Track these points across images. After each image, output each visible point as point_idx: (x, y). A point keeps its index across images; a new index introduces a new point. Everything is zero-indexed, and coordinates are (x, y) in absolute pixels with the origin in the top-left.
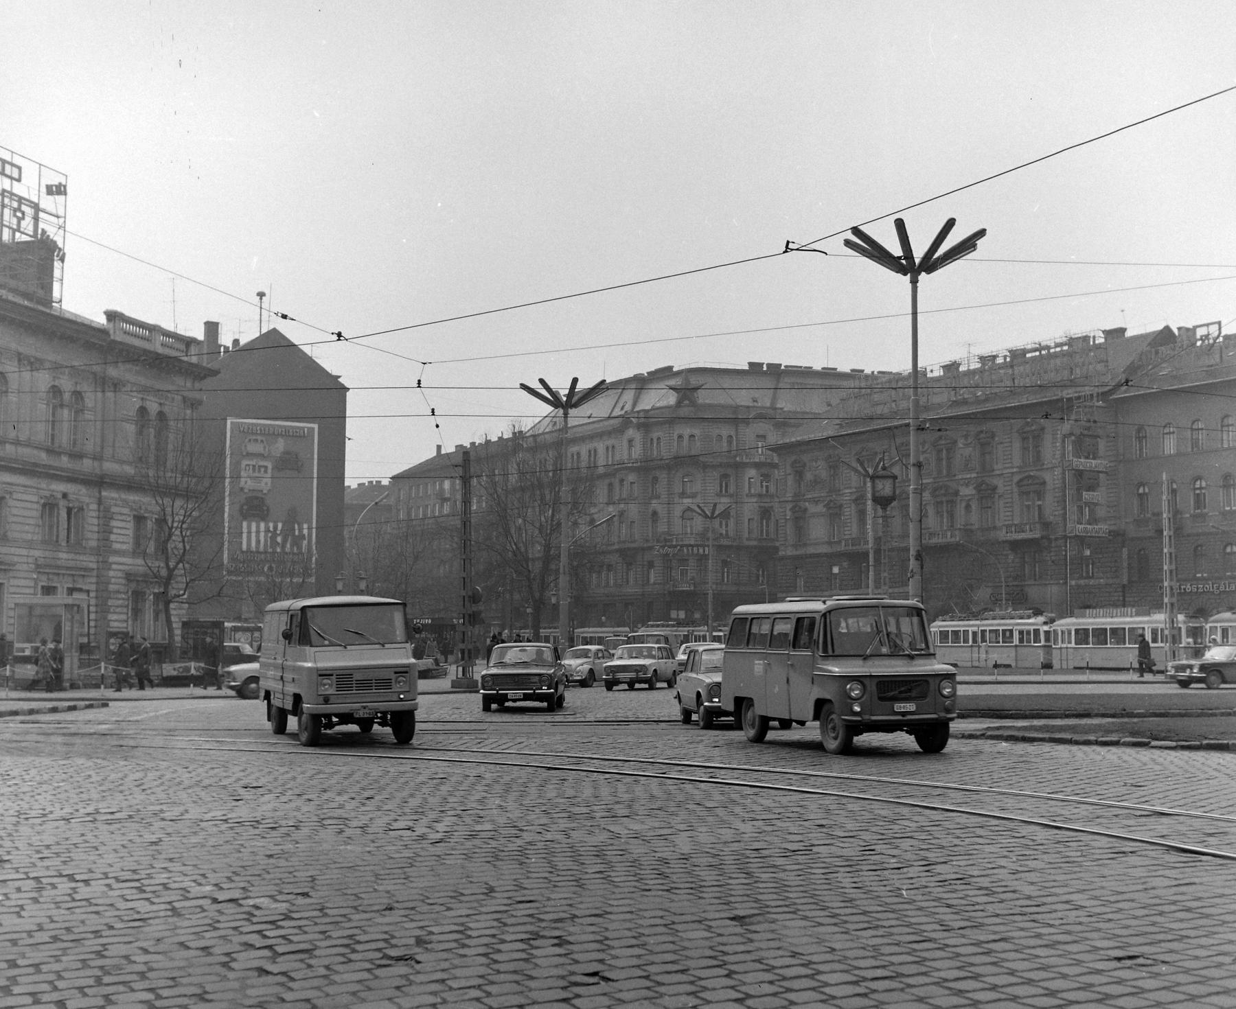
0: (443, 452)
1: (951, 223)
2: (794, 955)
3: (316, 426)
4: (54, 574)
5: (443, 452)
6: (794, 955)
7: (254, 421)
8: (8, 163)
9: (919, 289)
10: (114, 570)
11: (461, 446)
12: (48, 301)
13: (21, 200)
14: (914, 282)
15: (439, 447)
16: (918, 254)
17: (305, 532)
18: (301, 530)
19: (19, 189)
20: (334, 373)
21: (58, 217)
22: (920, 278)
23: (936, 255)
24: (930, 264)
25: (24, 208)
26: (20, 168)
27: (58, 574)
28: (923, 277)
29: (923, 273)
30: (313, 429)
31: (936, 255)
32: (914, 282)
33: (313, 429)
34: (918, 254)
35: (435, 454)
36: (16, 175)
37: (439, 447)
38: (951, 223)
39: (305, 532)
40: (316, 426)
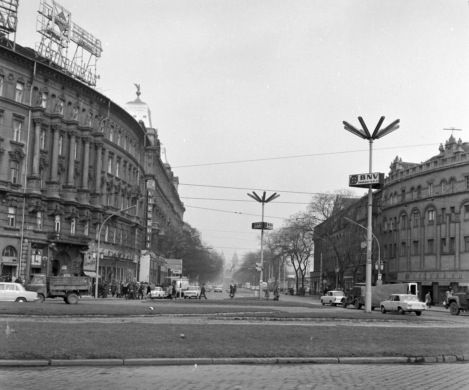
1: (382, 119)
14: (371, 142)
24: (377, 135)
32: (371, 142)
38: (382, 119)
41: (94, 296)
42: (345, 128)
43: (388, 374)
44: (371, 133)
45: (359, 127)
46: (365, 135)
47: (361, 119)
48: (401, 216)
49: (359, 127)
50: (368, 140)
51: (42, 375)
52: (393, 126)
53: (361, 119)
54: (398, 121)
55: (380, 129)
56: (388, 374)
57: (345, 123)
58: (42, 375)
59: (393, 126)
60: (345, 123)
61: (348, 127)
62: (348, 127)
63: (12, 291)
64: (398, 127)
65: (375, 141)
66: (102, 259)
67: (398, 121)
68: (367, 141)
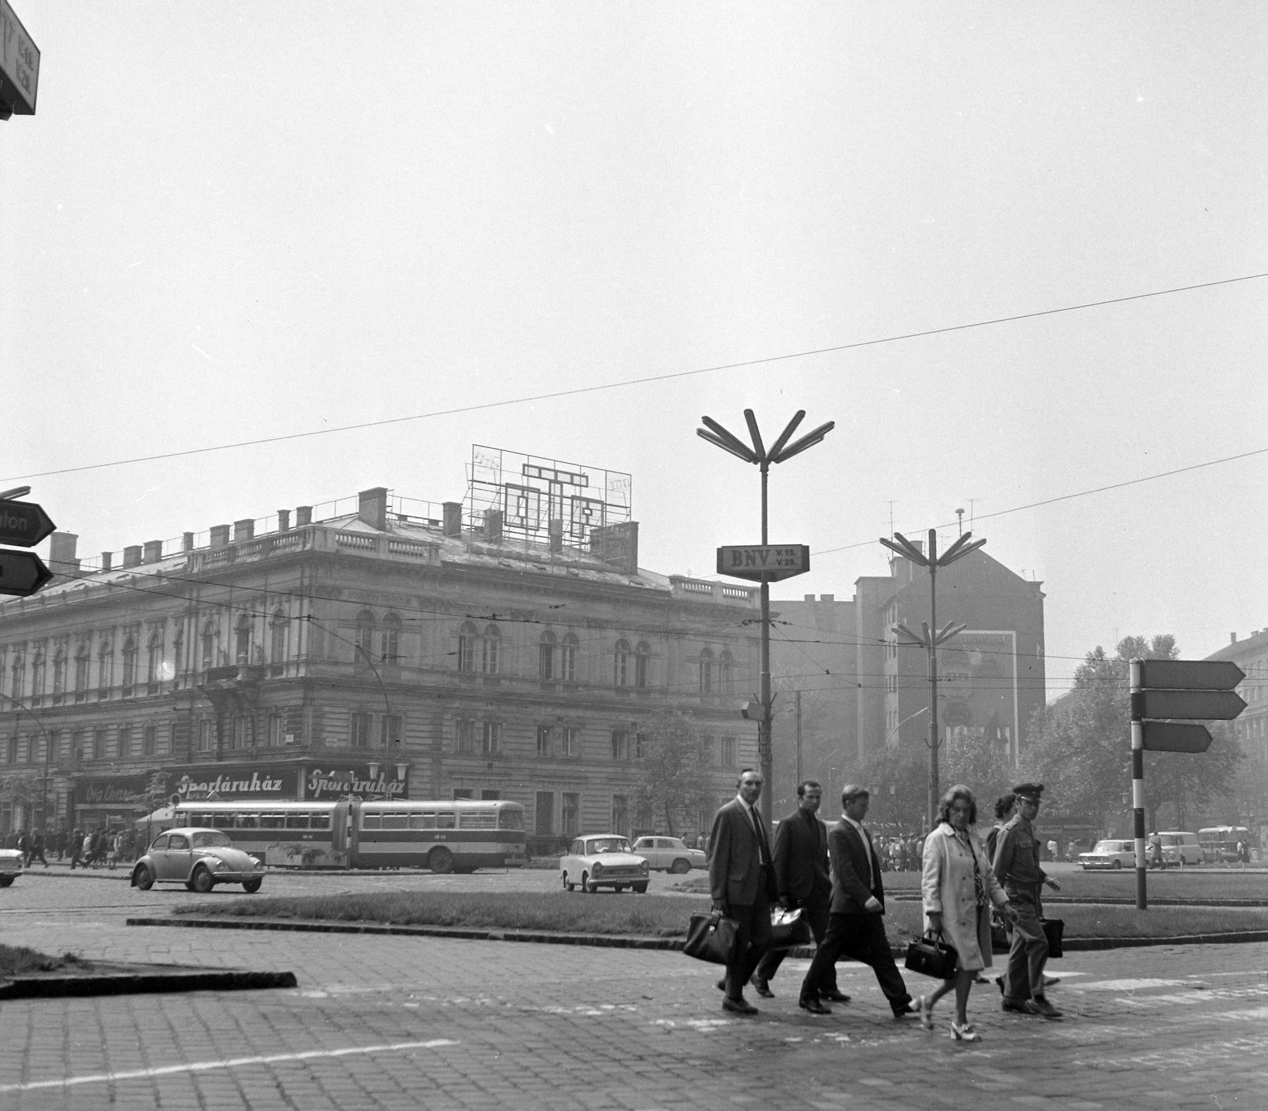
0: (1238, 639)
1: (800, 415)
2: (515, 1085)
3: (1013, 633)
4: (549, 782)
5: (1238, 639)
6: (515, 1085)
7: (989, 632)
8: (577, 475)
9: (769, 478)
10: (427, 776)
11: (1257, 632)
12: (632, 570)
13: (588, 500)
14: (764, 471)
15: (1233, 635)
16: (768, 447)
17: (1008, 734)
18: (1003, 734)
19: (586, 493)
20: (1028, 578)
21: (626, 508)
22: (770, 466)
23: (787, 445)
24: (779, 454)
25: (592, 505)
26: (587, 477)
27: (553, 782)
28: (772, 465)
29: (773, 463)
30: (1011, 635)
31: (787, 445)
32: (764, 471)
33: (1011, 635)
34: (768, 447)
35: (1230, 643)
36: (584, 483)
37: (1233, 635)
38: (800, 415)
39: (1008, 734)
40: (1013, 633)
47: (749, 415)
53: (749, 415)
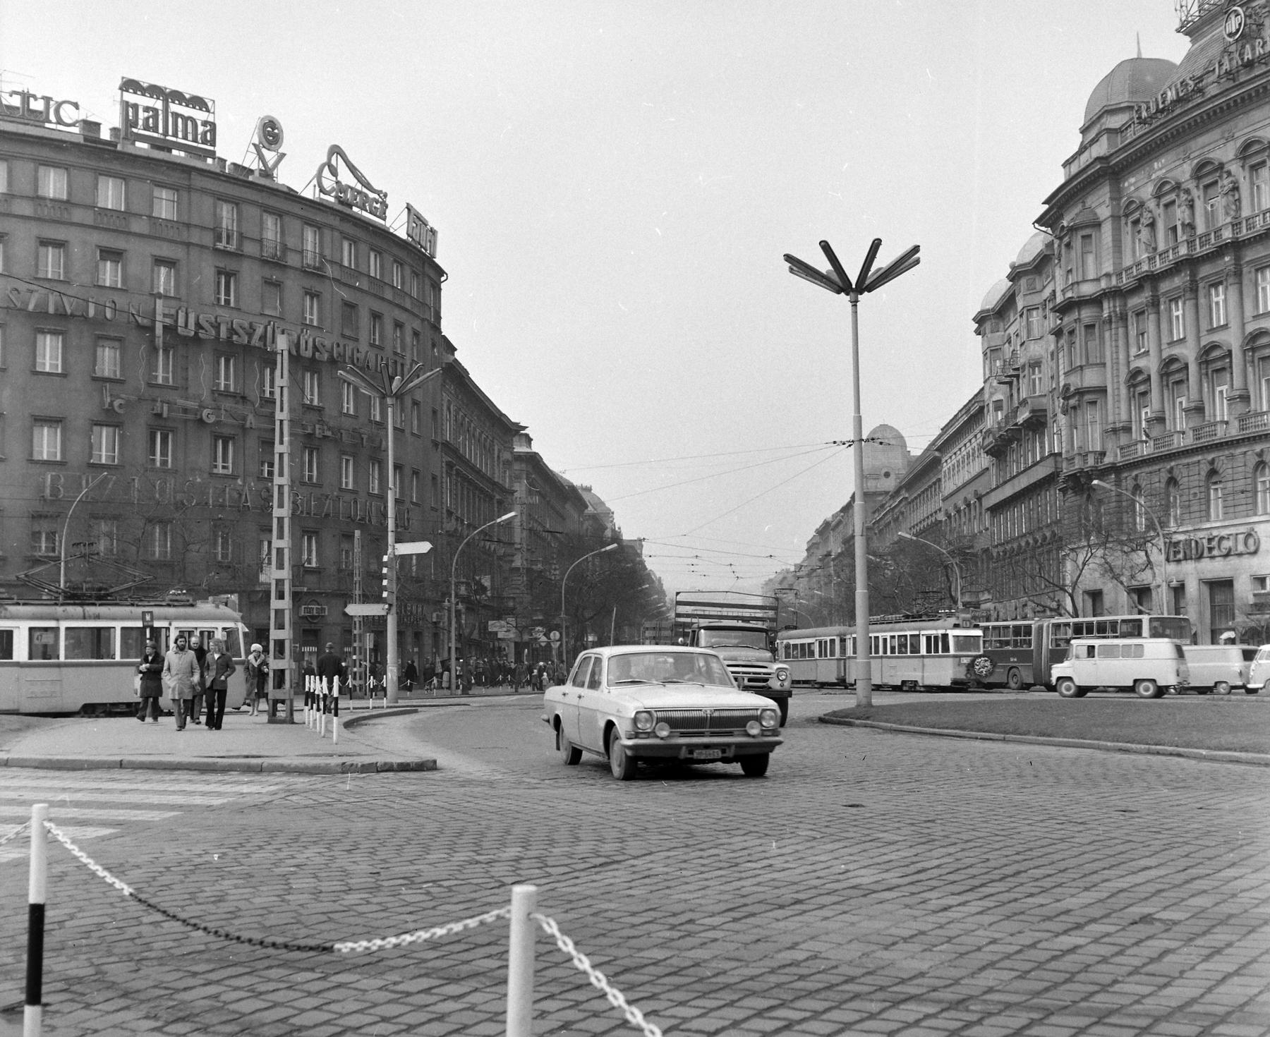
1: (876, 245)
14: (855, 303)
24: (866, 284)
38: (876, 245)
41: (1174, 584)
42: (791, 270)
43: (989, 978)
44: (853, 277)
45: (824, 266)
46: (838, 282)
47: (826, 247)
48: (1063, 247)
49: (824, 266)
50: (847, 294)
51: (212, 990)
52: (908, 260)
53: (826, 247)
54: (916, 249)
55: (873, 269)
56: (989, 978)
57: (788, 258)
58: (212, 990)
59: (908, 260)
60: (788, 258)
61: (798, 266)
62: (798, 266)
63: (932, 632)
64: (917, 262)
65: (864, 298)
66: (599, 639)
67: (916, 249)
68: (844, 298)
